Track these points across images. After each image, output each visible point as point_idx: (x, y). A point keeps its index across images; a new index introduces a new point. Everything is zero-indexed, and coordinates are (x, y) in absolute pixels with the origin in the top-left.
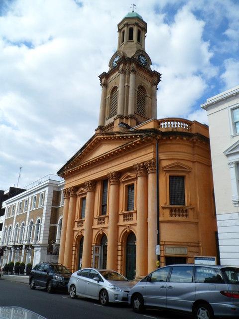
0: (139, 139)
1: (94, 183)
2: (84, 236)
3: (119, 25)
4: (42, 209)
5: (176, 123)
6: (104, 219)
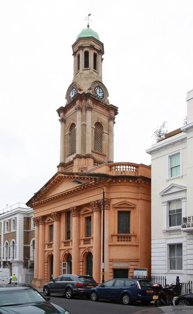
0: (94, 182)
1: (59, 214)
2: (54, 254)
3: (73, 46)
4: (15, 233)
5: (130, 167)
6: (69, 242)
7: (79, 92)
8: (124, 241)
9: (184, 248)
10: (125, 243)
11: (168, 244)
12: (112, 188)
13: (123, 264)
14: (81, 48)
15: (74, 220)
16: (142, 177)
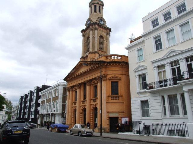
1: (80, 85)
3: (89, 4)
4: (58, 96)
7: (91, 22)
8: (115, 99)
9: (149, 103)
10: (116, 101)
11: (140, 101)
12: (108, 68)
13: (115, 114)
14: (93, 4)
15: (88, 88)
16: (123, 62)
